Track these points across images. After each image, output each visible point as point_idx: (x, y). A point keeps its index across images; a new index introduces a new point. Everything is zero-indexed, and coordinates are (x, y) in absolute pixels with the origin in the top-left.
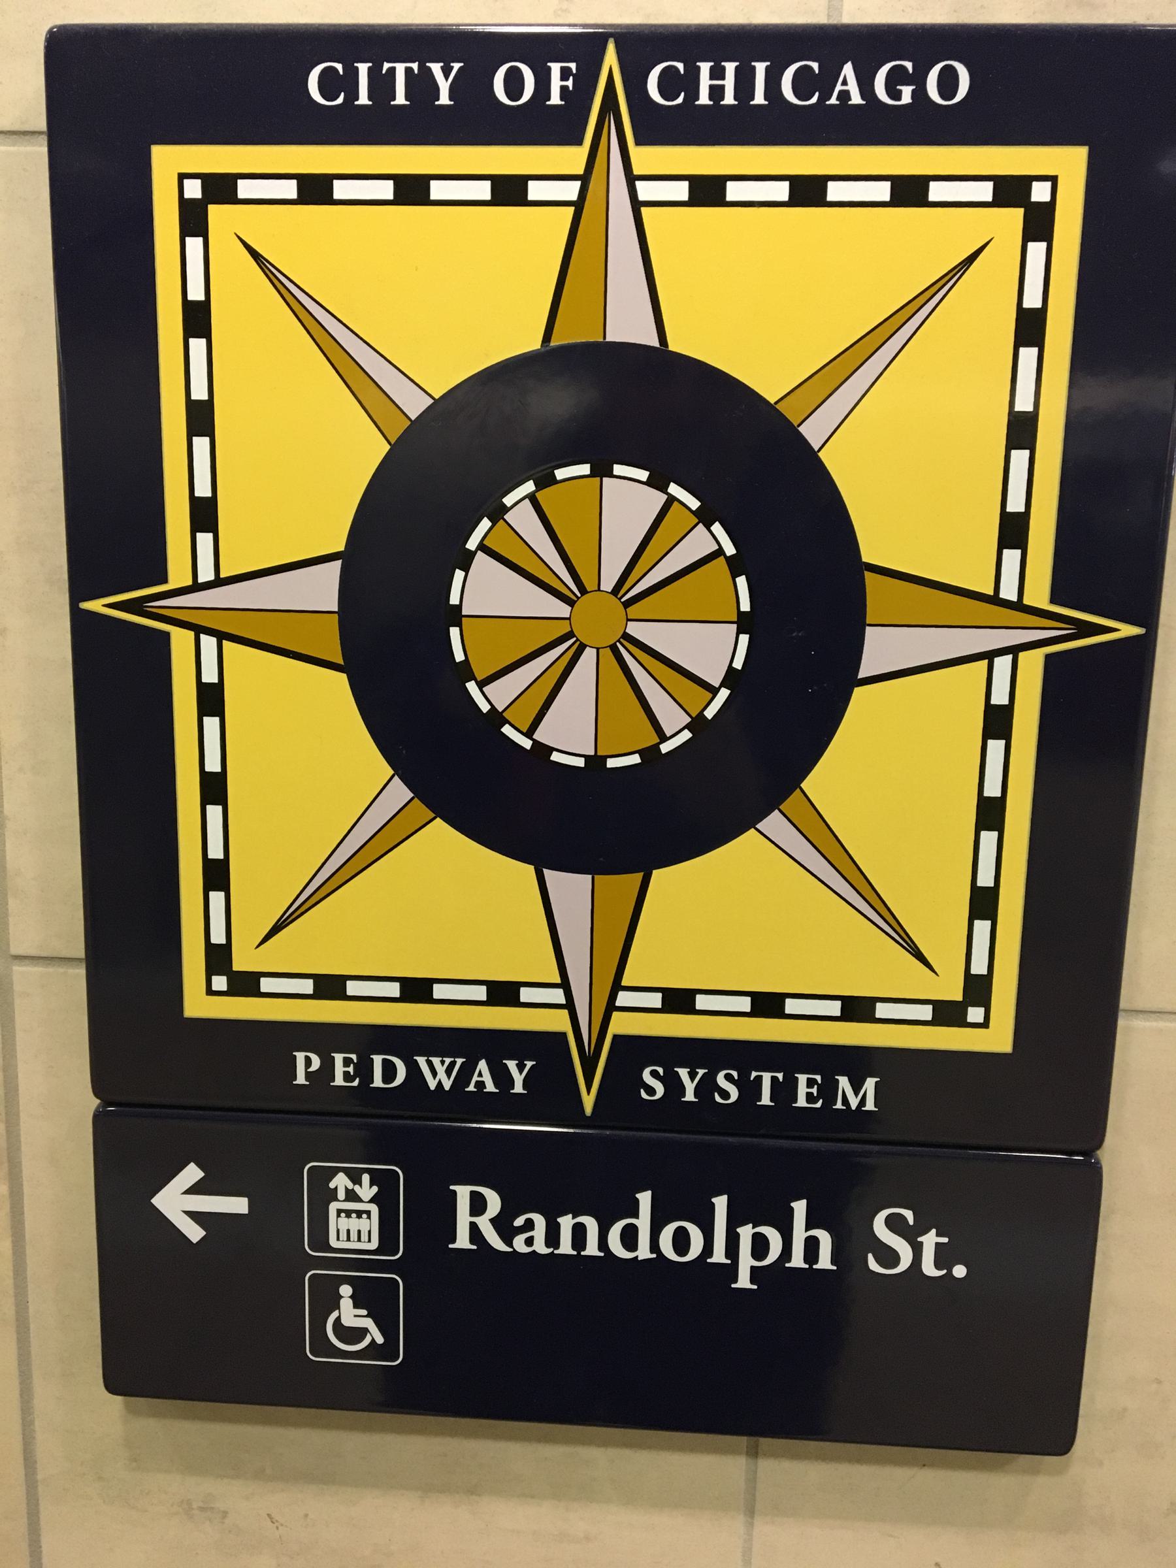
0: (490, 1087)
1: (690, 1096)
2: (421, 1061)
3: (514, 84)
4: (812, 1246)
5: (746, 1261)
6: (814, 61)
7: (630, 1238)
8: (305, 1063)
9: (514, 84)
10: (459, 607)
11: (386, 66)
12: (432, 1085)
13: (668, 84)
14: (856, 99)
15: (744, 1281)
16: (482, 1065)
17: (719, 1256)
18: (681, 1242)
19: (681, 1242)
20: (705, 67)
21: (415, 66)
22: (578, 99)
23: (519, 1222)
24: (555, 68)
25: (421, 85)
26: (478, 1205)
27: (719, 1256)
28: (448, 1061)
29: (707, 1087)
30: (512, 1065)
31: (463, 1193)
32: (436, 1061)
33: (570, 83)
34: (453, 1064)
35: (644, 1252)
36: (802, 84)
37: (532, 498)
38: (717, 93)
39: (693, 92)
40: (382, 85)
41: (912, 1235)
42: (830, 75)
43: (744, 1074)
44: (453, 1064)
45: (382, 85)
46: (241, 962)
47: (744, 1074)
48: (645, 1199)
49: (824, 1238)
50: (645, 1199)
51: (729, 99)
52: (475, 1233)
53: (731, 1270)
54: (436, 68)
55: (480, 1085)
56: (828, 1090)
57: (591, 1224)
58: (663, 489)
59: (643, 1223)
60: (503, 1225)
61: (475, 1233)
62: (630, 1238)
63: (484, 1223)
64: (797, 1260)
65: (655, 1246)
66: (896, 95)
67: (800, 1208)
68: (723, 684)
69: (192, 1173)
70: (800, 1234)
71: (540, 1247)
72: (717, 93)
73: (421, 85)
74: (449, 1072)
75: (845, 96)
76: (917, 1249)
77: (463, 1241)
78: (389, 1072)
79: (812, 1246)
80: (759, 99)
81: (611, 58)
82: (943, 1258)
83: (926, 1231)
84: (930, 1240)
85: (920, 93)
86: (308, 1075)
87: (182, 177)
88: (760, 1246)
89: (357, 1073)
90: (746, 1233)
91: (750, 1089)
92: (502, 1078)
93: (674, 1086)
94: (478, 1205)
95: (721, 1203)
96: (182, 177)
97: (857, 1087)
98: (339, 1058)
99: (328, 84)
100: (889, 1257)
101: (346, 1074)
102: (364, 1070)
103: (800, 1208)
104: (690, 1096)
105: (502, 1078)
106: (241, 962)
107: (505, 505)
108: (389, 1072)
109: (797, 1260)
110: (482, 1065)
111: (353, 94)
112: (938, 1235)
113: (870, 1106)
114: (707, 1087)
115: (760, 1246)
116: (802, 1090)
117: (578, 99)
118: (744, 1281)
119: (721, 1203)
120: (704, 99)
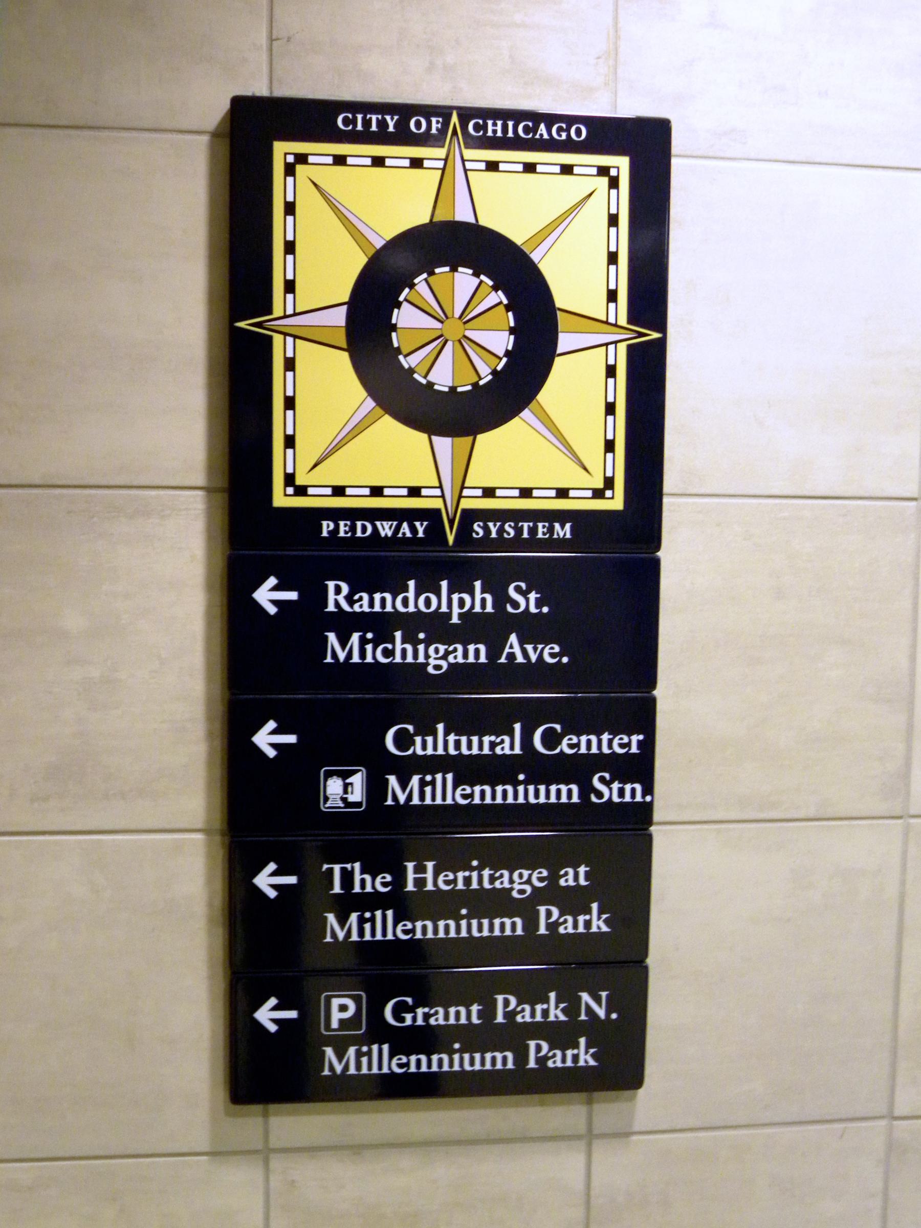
0: (408, 535)
1: (494, 535)
2: (378, 523)
3: (418, 125)
4: (483, 601)
5: (456, 610)
6: (530, 122)
7: (405, 602)
8: (327, 527)
9: (418, 125)
10: (396, 325)
11: (369, 116)
12: (383, 534)
13: (477, 127)
14: (546, 136)
15: (455, 620)
16: (405, 525)
17: (444, 609)
18: (428, 603)
19: (428, 603)
20: (490, 123)
21: (380, 117)
22: (443, 131)
23: (356, 597)
24: (434, 120)
25: (382, 124)
26: (338, 590)
27: (444, 609)
28: (390, 523)
29: (501, 531)
30: (417, 524)
31: (331, 585)
32: (385, 523)
33: (439, 126)
34: (392, 525)
35: (411, 609)
36: (526, 130)
37: (426, 280)
38: (495, 132)
39: (486, 131)
40: (367, 123)
41: (524, 594)
42: (535, 129)
43: (516, 524)
44: (392, 525)
45: (367, 123)
46: (299, 481)
47: (516, 524)
48: (412, 584)
49: (489, 597)
50: (412, 584)
51: (499, 134)
52: (337, 604)
53: (449, 615)
54: (388, 118)
55: (404, 534)
56: (551, 530)
57: (388, 596)
58: (478, 276)
59: (411, 594)
60: (350, 600)
61: (337, 604)
62: (405, 602)
63: (341, 599)
64: (478, 609)
65: (416, 606)
66: (560, 136)
67: (478, 584)
68: (504, 356)
69: (272, 581)
70: (478, 596)
71: (366, 609)
72: (495, 132)
73: (382, 124)
74: (390, 528)
75: (541, 135)
76: (527, 600)
77: (331, 608)
78: (364, 529)
79: (483, 601)
80: (510, 134)
81: (455, 119)
82: (539, 604)
83: (530, 592)
84: (533, 596)
85: (569, 136)
86: (329, 532)
87: (286, 154)
88: (462, 603)
89: (548, 529)
90: (455, 597)
91: (519, 531)
92: (414, 530)
93: (487, 530)
94: (338, 590)
95: (444, 584)
96: (286, 154)
97: (563, 527)
98: (342, 523)
99: (346, 121)
100: (516, 605)
101: (345, 531)
102: (353, 529)
103: (478, 584)
104: (494, 535)
105: (414, 530)
106: (299, 481)
107: (289, 293)
108: (364, 529)
109: (478, 609)
110: (405, 525)
111: (355, 125)
112: (536, 593)
113: (568, 536)
114: (501, 531)
115: (462, 603)
116: (540, 530)
117: (443, 131)
118: (455, 620)
119: (444, 584)
120: (490, 133)
